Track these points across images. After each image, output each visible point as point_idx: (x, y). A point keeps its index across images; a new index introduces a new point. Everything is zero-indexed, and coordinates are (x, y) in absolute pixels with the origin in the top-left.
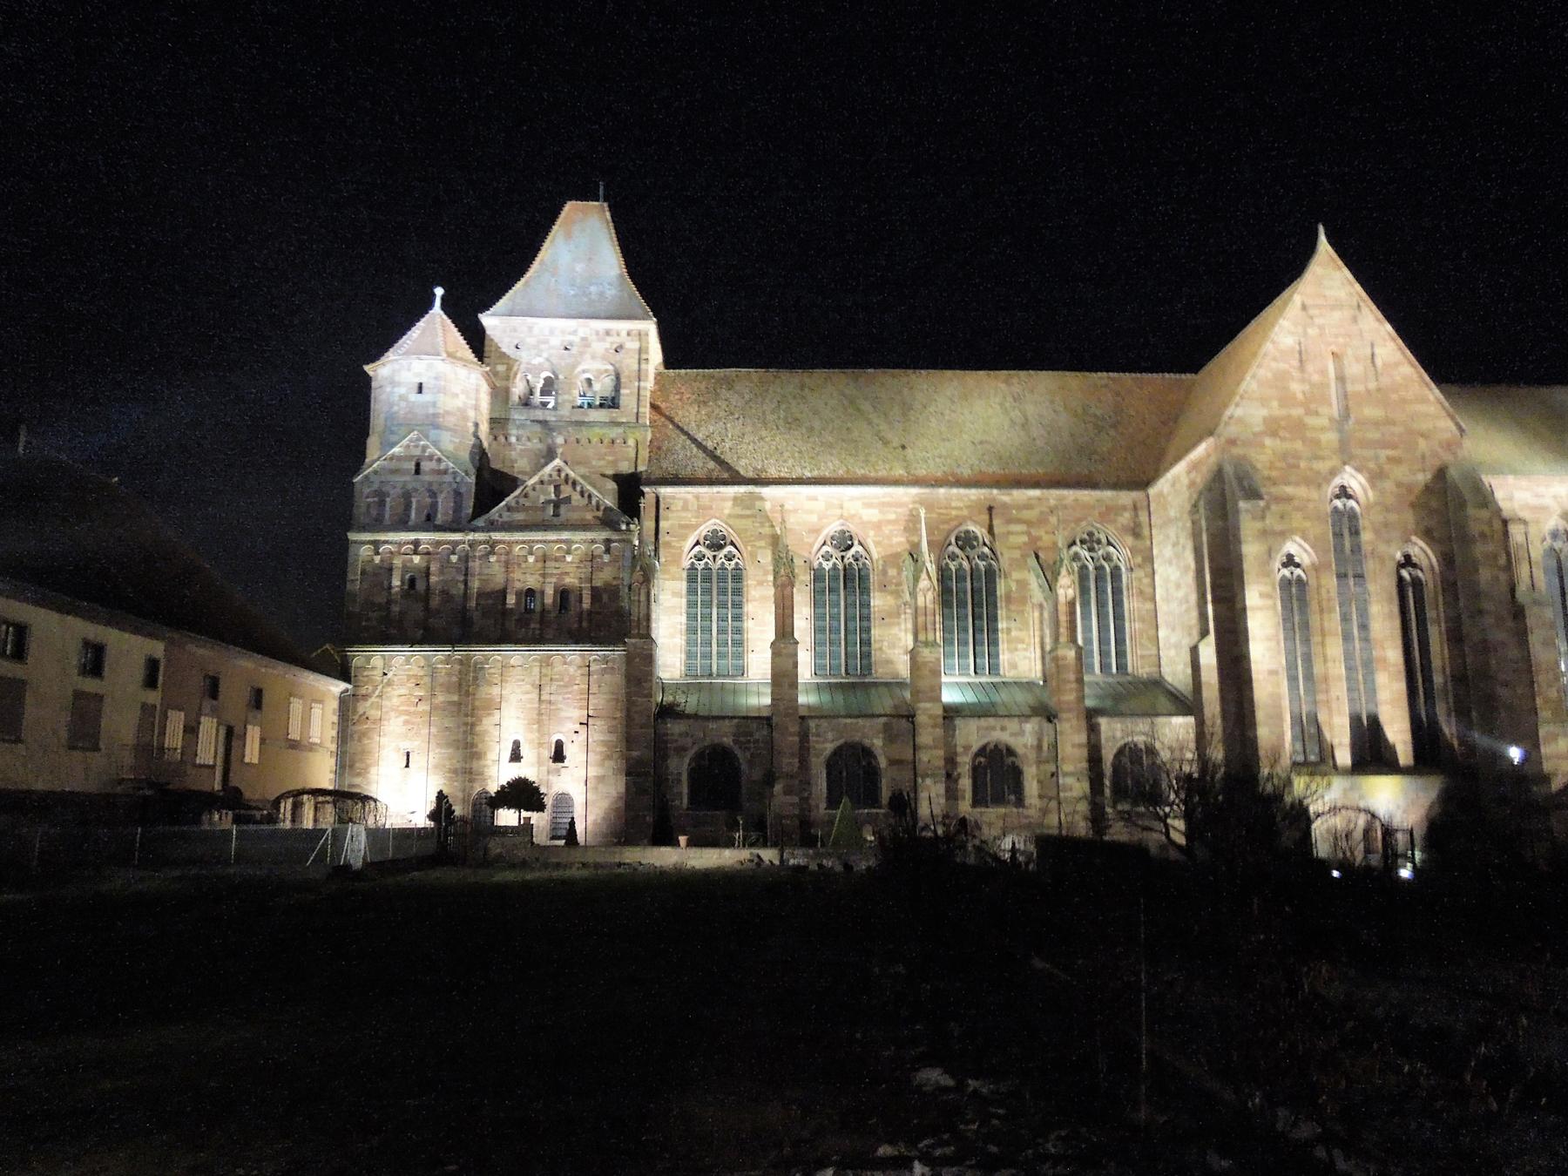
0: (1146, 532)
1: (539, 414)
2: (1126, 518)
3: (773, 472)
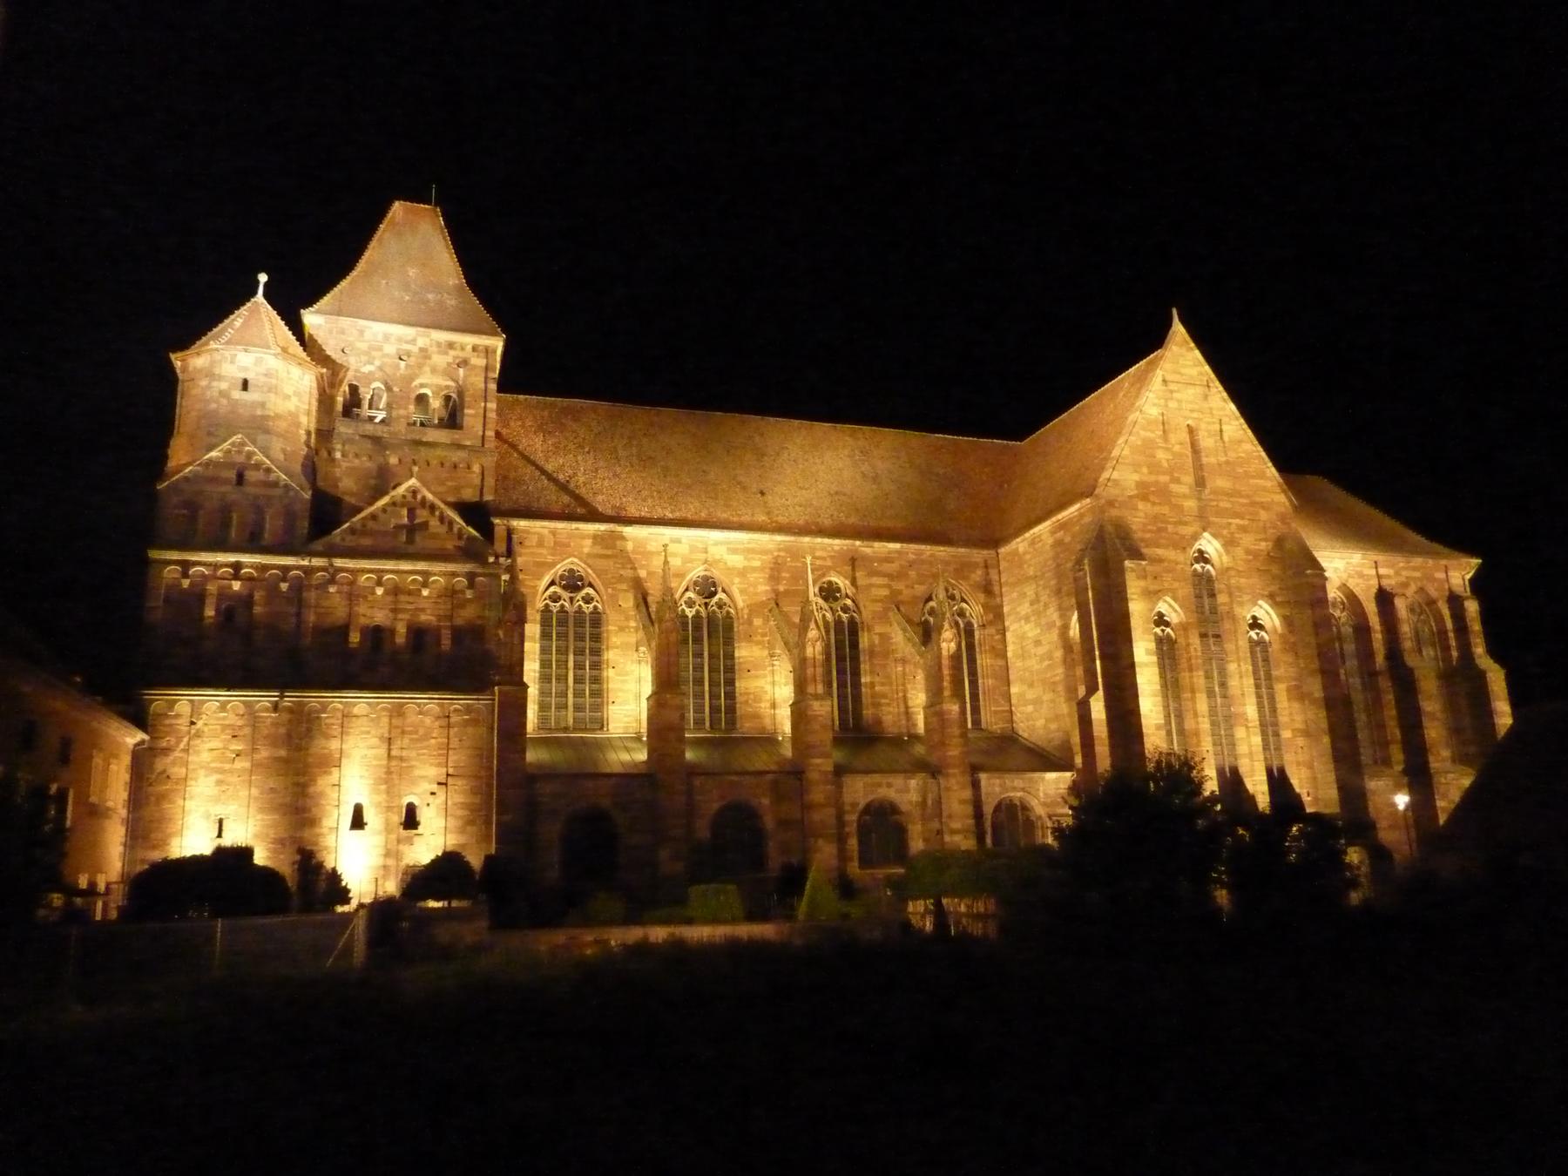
0: (996, 589)
1: (369, 428)
2: (978, 575)
3: (633, 511)
